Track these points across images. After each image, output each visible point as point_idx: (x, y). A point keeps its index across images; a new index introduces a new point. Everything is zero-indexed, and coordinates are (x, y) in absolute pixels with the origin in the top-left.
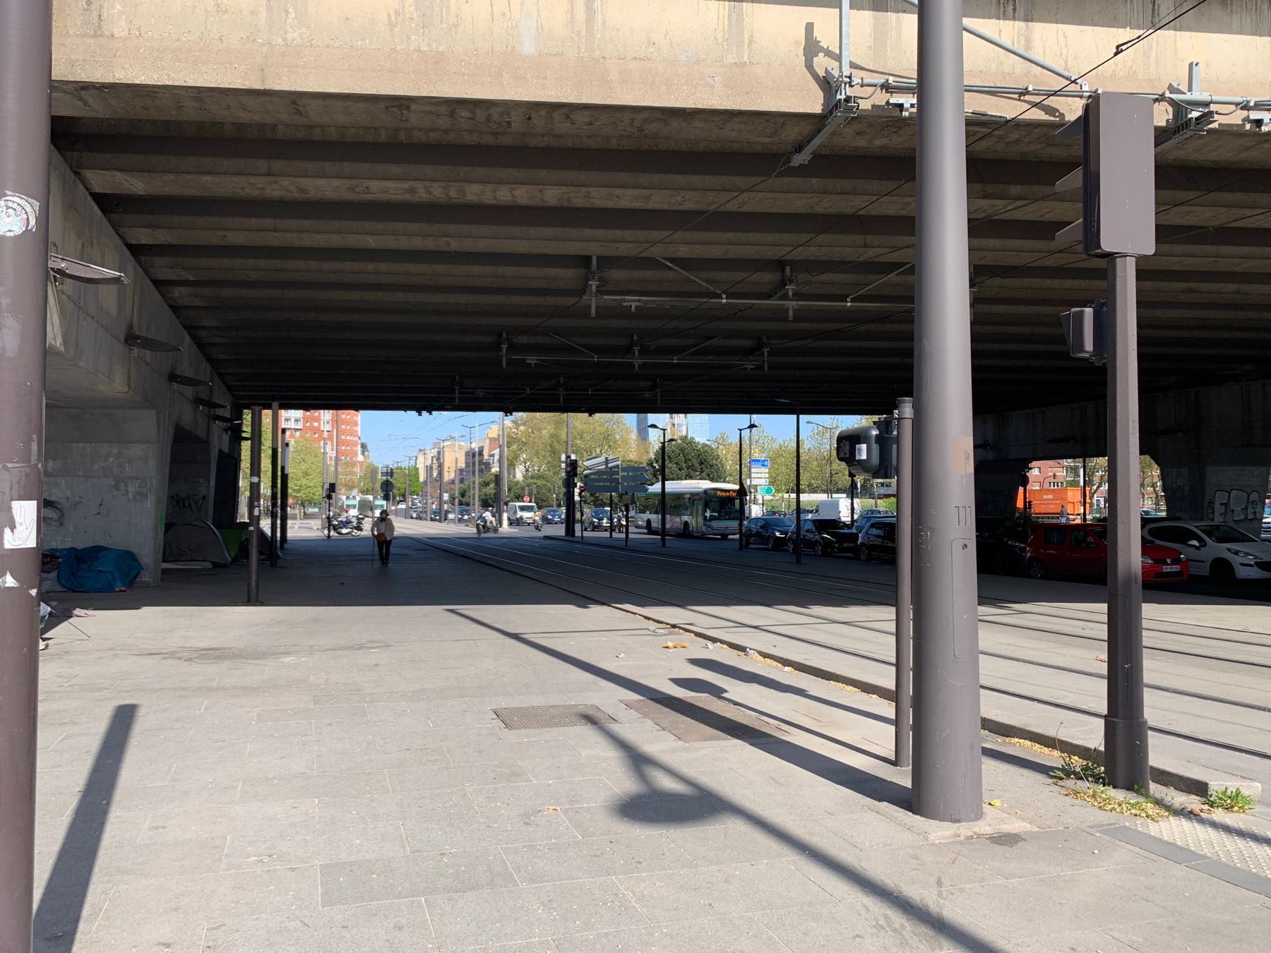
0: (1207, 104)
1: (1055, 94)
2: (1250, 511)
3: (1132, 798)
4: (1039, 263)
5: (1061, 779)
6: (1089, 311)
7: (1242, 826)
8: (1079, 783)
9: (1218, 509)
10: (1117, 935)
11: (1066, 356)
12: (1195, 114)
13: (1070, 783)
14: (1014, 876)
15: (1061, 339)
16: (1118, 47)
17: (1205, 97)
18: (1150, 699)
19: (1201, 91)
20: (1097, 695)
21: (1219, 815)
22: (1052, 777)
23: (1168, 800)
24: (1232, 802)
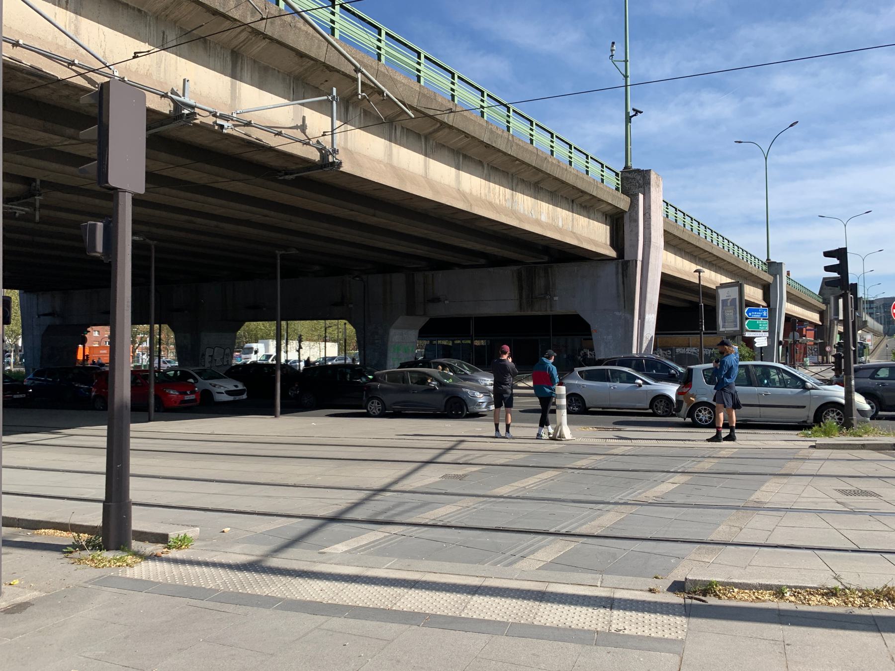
0: (193, 107)
1: (93, 71)
2: (225, 360)
3: (118, 554)
4: (88, 187)
5: (71, 552)
6: (100, 225)
7: (185, 557)
8: (83, 553)
9: (208, 359)
10: (87, 655)
11: (83, 250)
12: (186, 112)
13: (77, 554)
14: (17, 635)
15: (79, 242)
16: (135, 53)
17: (192, 102)
18: (134, 484)
19: (190, 99)
20: (98, 487)
21: (174, 554)
22: (65, 553)
23: (142, 550)
24: (183, 542)
